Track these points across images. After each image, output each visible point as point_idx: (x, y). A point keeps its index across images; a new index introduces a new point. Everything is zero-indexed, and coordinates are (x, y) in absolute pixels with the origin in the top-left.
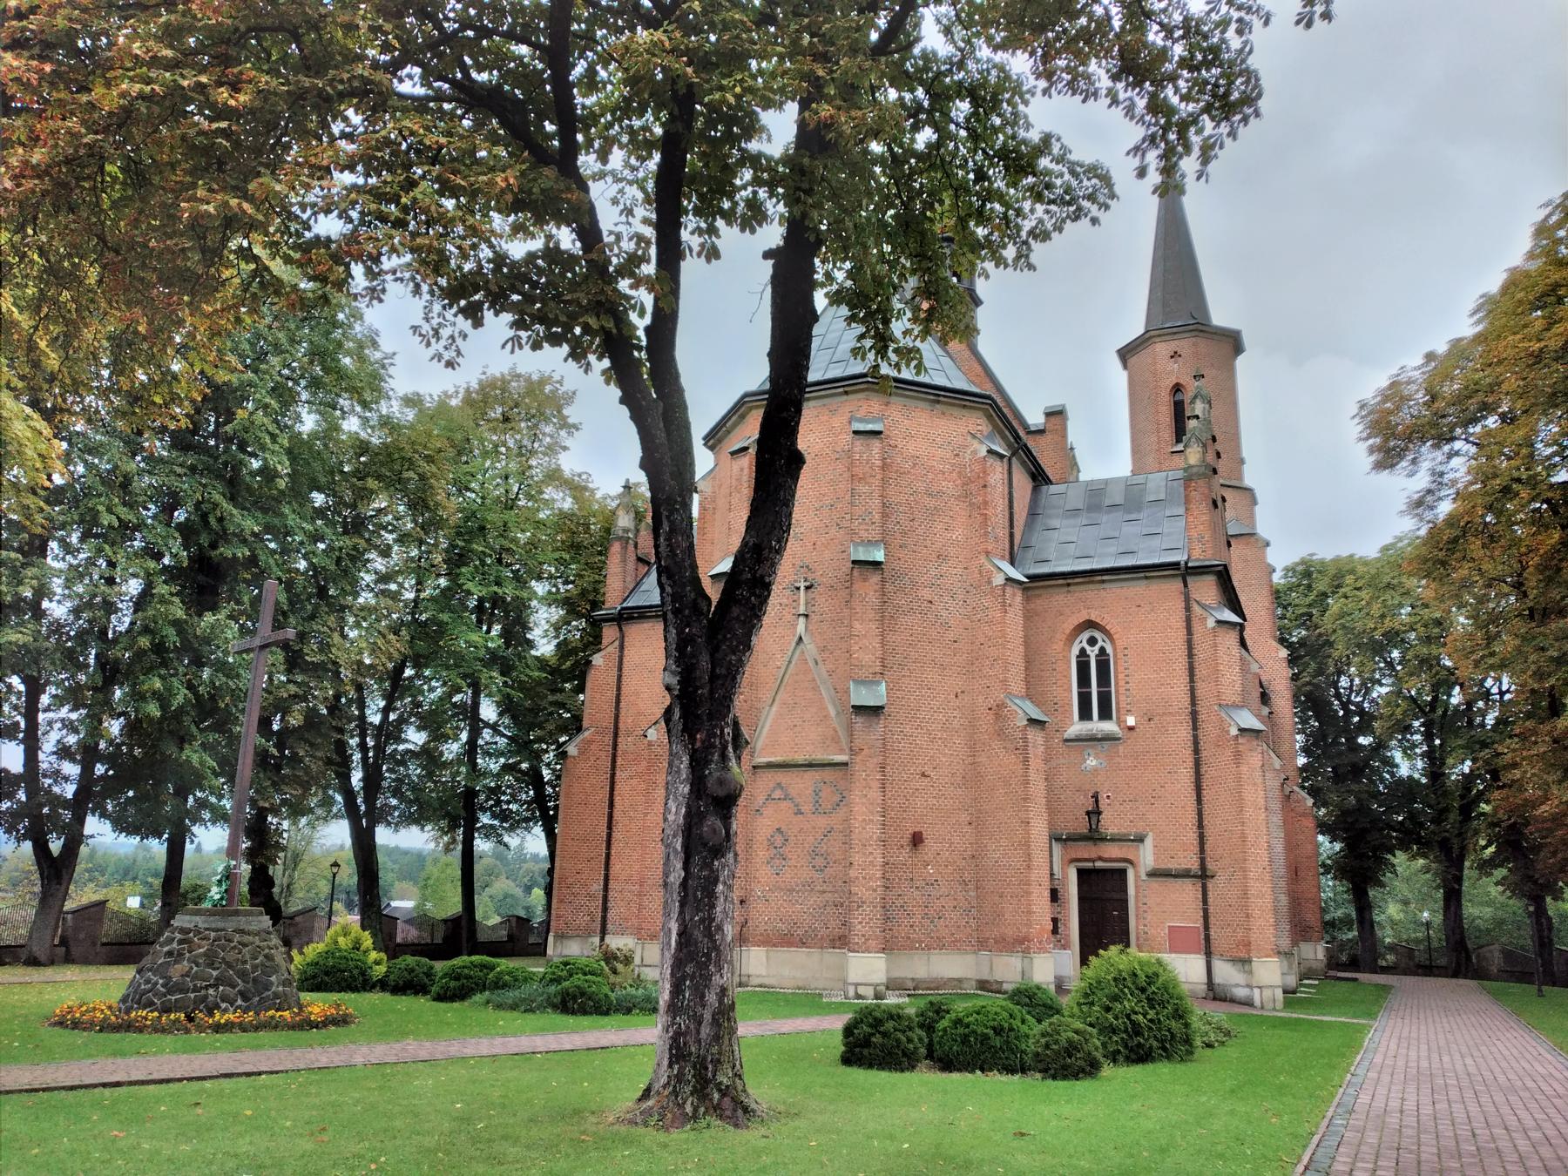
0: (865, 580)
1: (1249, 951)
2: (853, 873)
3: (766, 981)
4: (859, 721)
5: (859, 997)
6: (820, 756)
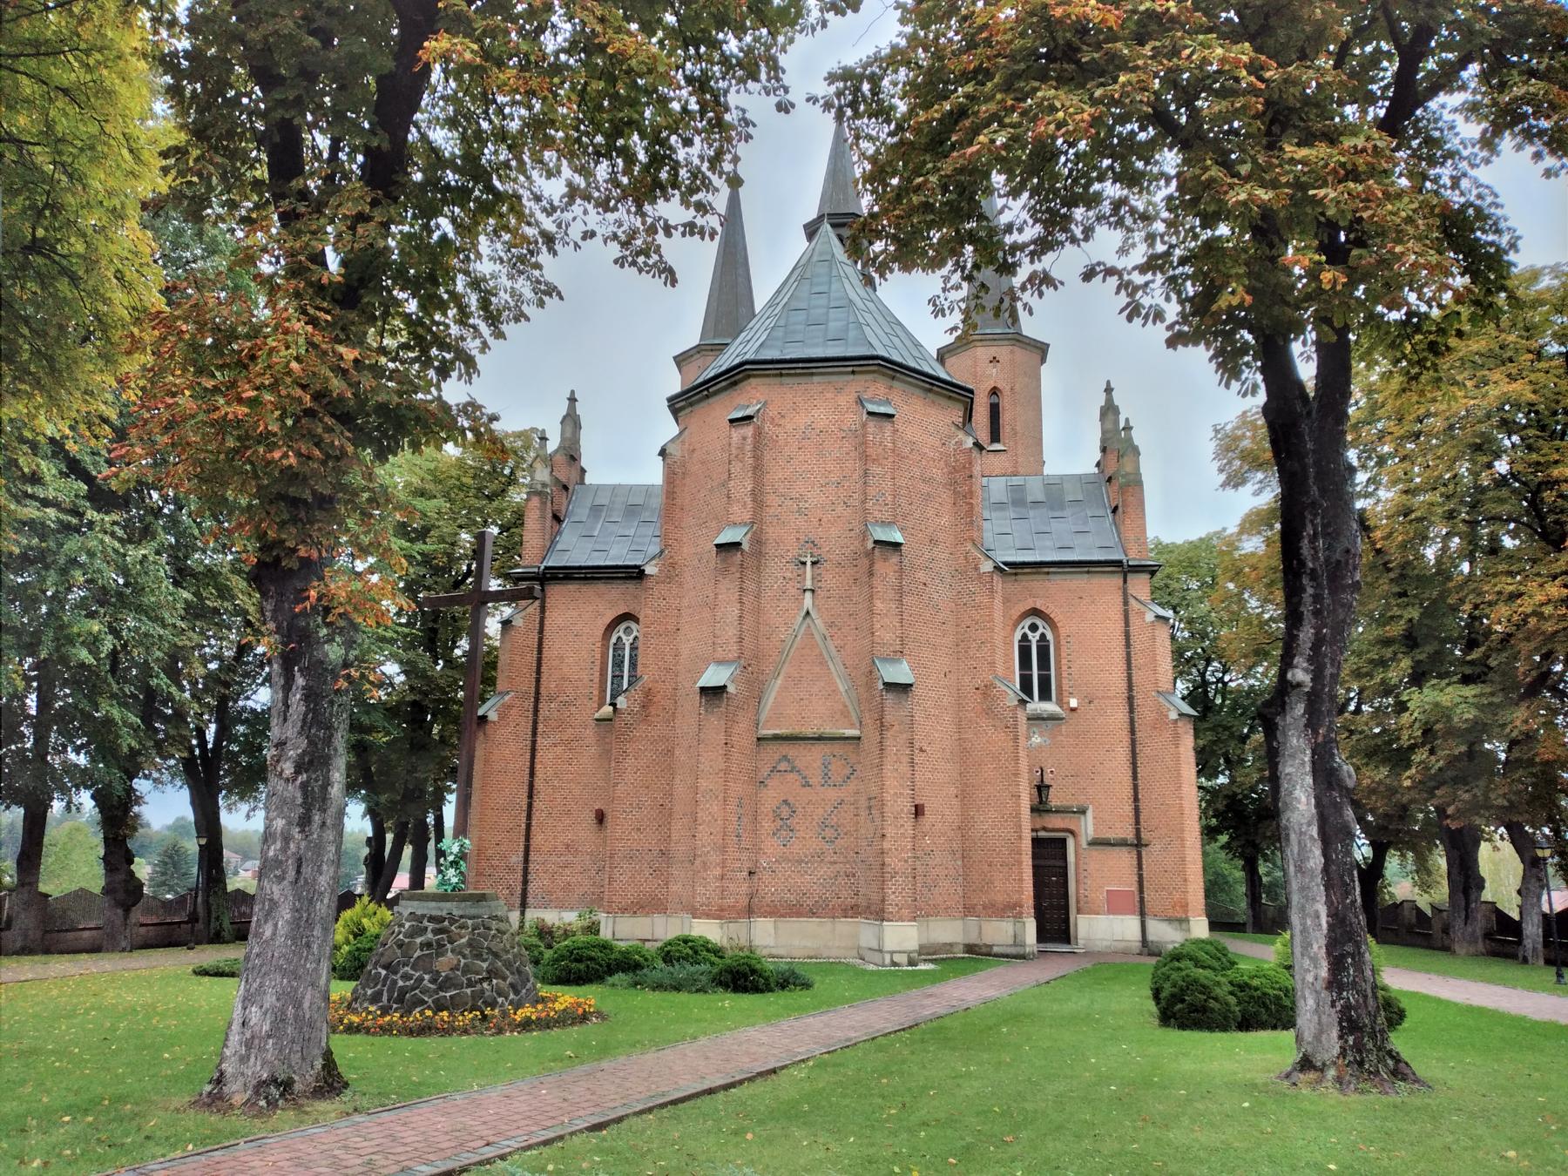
0: (885, 560)
1: (1186, 912)
2: (886, 845)
3: (774, 952)
4: (890, 698)
5: (894, 964)
6: (829, 730)
